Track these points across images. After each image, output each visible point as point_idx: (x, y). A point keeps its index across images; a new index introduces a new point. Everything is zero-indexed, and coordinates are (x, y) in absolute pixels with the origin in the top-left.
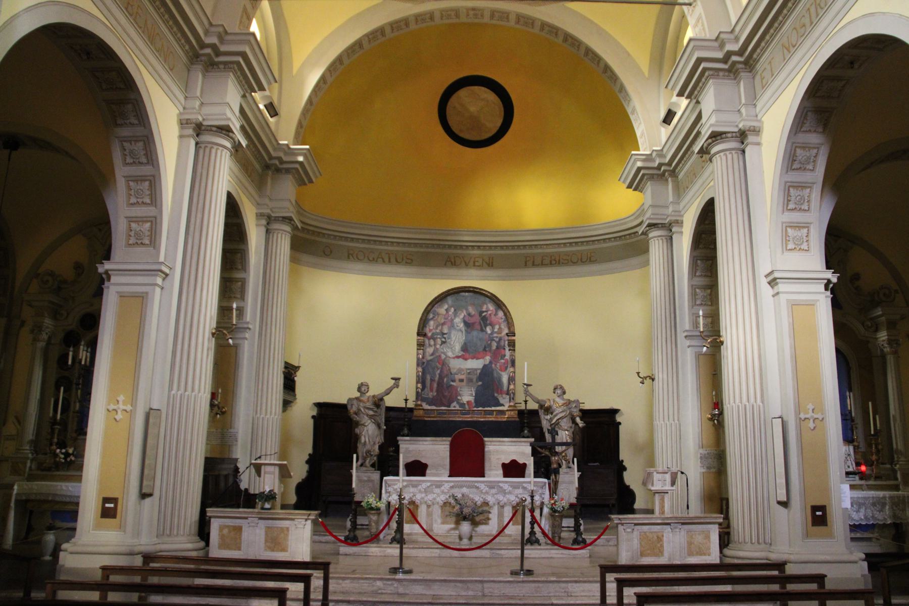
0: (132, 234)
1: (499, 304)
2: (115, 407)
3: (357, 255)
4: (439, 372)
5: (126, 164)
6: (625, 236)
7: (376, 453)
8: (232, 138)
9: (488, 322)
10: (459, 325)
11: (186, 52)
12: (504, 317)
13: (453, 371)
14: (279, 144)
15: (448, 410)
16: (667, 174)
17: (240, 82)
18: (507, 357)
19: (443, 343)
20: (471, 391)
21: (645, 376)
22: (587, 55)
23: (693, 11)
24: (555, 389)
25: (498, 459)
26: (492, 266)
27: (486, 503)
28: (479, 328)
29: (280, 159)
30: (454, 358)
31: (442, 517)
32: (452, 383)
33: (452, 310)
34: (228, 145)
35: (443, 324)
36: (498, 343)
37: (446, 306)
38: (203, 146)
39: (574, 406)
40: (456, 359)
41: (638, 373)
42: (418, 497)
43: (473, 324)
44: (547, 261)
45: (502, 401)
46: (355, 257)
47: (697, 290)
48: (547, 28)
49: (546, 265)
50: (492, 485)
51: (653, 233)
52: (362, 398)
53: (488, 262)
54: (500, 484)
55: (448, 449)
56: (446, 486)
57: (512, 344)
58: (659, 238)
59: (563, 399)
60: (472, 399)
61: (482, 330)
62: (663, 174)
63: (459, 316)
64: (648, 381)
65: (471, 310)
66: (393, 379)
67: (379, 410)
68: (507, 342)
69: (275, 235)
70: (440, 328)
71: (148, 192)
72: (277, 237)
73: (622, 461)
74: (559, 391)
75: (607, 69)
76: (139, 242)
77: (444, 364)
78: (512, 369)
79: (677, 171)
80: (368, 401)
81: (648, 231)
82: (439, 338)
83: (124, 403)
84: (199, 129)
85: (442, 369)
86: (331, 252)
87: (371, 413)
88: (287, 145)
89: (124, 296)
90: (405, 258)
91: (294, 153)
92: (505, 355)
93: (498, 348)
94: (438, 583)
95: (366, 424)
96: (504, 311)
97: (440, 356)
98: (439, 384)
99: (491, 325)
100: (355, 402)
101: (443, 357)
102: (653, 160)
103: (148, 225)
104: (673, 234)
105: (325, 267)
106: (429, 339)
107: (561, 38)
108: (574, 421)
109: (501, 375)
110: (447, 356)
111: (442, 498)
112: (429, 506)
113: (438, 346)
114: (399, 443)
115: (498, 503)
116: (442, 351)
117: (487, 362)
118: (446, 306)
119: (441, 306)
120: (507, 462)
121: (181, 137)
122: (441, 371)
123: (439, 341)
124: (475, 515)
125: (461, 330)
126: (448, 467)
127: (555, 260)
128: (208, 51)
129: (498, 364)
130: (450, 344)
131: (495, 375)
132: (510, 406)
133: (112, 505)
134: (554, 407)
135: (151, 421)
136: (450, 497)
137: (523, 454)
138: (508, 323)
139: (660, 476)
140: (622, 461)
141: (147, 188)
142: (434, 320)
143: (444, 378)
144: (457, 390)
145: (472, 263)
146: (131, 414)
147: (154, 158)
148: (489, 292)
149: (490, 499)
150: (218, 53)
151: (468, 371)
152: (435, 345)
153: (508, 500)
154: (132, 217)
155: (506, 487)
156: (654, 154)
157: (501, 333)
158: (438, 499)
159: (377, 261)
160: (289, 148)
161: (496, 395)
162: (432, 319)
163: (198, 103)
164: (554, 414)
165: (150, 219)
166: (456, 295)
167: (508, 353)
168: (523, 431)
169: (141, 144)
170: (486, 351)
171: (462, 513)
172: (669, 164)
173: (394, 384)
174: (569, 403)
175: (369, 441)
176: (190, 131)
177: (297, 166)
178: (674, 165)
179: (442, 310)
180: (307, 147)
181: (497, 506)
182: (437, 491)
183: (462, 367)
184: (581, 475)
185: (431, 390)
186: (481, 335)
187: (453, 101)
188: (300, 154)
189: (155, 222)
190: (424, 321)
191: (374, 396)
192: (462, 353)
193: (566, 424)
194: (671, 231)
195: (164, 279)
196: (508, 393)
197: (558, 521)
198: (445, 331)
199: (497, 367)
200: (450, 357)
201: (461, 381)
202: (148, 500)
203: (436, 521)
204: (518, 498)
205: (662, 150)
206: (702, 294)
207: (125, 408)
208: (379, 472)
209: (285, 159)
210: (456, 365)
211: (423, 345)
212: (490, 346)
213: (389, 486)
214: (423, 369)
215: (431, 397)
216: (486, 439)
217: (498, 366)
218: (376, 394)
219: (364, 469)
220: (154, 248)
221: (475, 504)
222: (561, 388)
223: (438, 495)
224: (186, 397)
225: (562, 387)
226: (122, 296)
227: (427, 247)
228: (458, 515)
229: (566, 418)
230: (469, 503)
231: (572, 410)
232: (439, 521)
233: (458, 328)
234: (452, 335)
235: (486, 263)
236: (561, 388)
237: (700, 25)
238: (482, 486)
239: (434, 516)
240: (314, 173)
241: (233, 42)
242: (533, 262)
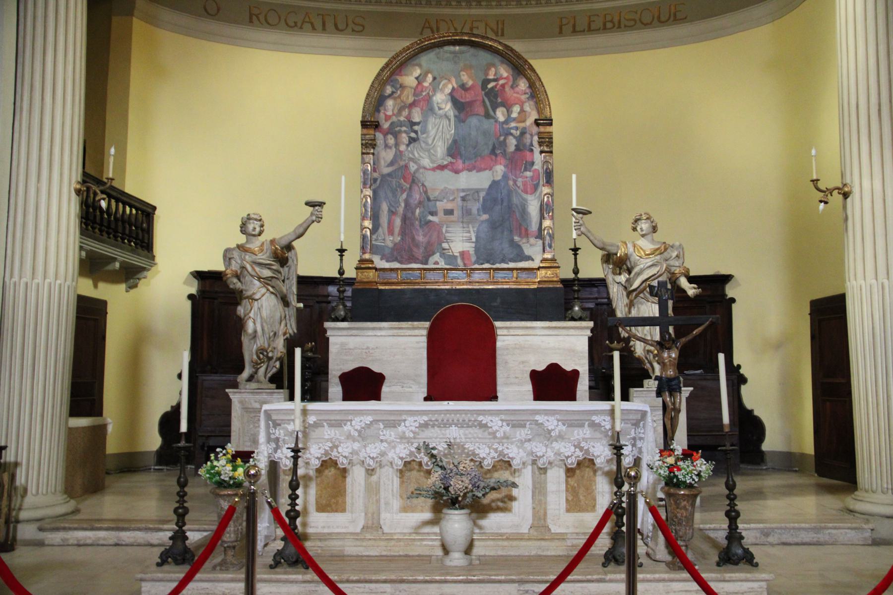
3: (266, 16)
4: (404, 196)
7: (279, 355)
9: (499, 100)
10: (443, 106)
12: (528, 91)
15: (425, 269)
18: (538, 166)
19: (412, 140)
20: (469, 232)
21: (831, 186)
25: (523, 362)
28: (481, 111)
30: (434, 169)
32: (430, 218)
33: (430, 78)
35: (412, 105)
37: (417, 72)
39: (674, 254)
40: (438, 171)
42: (343, 452)
43: (471, 104)
44: (598, 23)
45: (528, 251)
49: (597, 30)
50: (516, 421)
53: (495, 28)
54: (537, 417)
55: (425, 345)
56: (411, 423)
57: (547, 142)
59: (653, 241)
60: (469, 247)
63: (442, 90)
66: (307, 204)
67: (286, 269)
68: (536, 138)
70: (405, 113)
73: (739, 367)
74: (644, 226)
78: (546, 190)
80: (262, 250)
82: (405, 132)
86: (218, 10)
87: (267, 273)
90: (350, 22)
92: (533, 163)
93: (518, 148)
95: (257, 297)
96: (528, 79)
97: (406, 167)
98: (404, 219)
99: (504, 106)
100: (236, 254)
101: (413, 167)
106: (385, 134)
109: (526, 200)
110: (420, 167)
111: (401, 452)
112: (370, 472)
113: (403, 148)
114: (329, 333)
115: (534, 462)
116: (411, 155)
118: (417, 72)
120: (541, 367)
123: (404, 138)
124: (480, 495)
125: (447, 117)
126: (424, 379)
127: (612, 21)
129: (520, 180)
130: (427, 144)
134: (635, 257)
136: (418, 449)
137: (572, 351)
140: (739, 367)
142: (395, 99)
143: (416, 209)
144: (440, 232)
149: (516, 454)
151: (462, 194)
152: (397, 145)
153: (558, 454)
155: (551, 423)
157: (524, 121)
158: (391, 455)
159: (301, 28)
161: (516, 238)
162: (390, 96)
164: (636, 270)
166: (437, 50)
167: (538, 158)
168: (571, 308)
170: (496, 155)
171: (446, 489)
173: (312, 214)
174: (666, 249)
175: (263, 330)
179: (409, 79)
181: (530, 468)
182: (390, 434)
185: (391, 232)
186: (487, 124)
191: (272, 242)
192: (449, 159)
196: (540, 235)
197: (685, 508)
198: (417, 118)
200: (425, 168)
201: (449, 212)
203: (387, 504)
204: (581, 449)
211: (374, 146)
212: (504, 144)
213: (276, 425)
215: (390, 245)
216: (497, 324)
217: (519, 183)
218: (277, 236)
221: (480, 465)
222: (648, 218)
228: (437, 495)
230: (467, 465)
231: (672, 263)
232: (396, 504)
234: (430, 127)
235: (492, 29)
236: (648, 218)
238: (495, 423)
239: (382, 494)
242: (574, 26)
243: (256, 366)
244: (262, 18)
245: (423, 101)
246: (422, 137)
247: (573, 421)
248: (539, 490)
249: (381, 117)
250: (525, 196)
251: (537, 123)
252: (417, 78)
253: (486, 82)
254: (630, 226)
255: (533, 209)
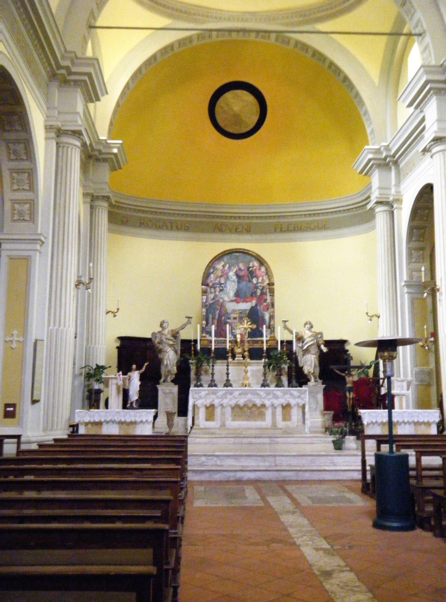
0: (16, 212)
1: (262, 262)
2: (11, 339)
3: (147, 223)
4: (218, 312)
5: (10, 160)
6: (352, 209)
8: (82, 139)
9: (254, 275)
10: (232, 277)
11: (47, 72)
13: (229, 311)
14: (99, 139)
16: (391, 163)
17: (84, 94)
19: (221, 290)
22: (330, 68)
23: (422, 40)
24: (306, 324)
26: (250, 231)
27: (263, 406)
28: (247, 279)
29: (99, 151)
30: (229, 302)
31: (232, 416)
33: (227, 266)
34: (78, 144)
35: (221, 277)
36: (262, 290)
37: (223, 263)
38: (62, 145)
41: (367, 313)
43: (243, 276)
46: (146, 225)
47: (413, 251)
48: (299, 46)
49: (291, 231)
51: (379, 209)
52: (163, 332)
57: (272, 292)
58: (384, 212)
59: (311, 331)
61: (250, 281)
62: (388, 164)
63: (232, 271)
64: (375, 319)
65: (241, 266)
66: (186, 317)
68: (268, 290)
69: (97, 210)
70: (218, 279)
71: (27, 181)
72: (99, 211)
74: (308, 326)
75: (346, 79)
76: (22, 218)
77: (222, 306)
78: (272, 310)
79: (399, 161)
81: (375, 206)
83: (18, 336)
84: (60, 133)
85: (220, 309)
88: (105, 140)
89: (12, 259)
91: (108, 146)
92: (266, 300)
94: (245, 458)
97: (219, 301)
101: (221, 301)
102: (381, 153)
103: (27, 206)
104: (394, 209)
105: (125, 234)
107: (310, 53)
108: (319, 346)
110: (224, 301)
111: (233, 402)
113: (217, 293)
117: (254, 305)
118: (223, 263)
119: (219, 263)
121: (46, 138)
122: (220, 312)
123: (218, 289)
128: (63, 71)
130: (227, 292)
131: (259, 313)
132: (270, 337)
133: (12, 409)
134: (305, 337)
135: (38, 348)
138: (269, 276)
139: (399, 383)
141: (26, 178)
145: (234, 229)
146: (23, 343)
147: (32, 156)
148: (254, 253)
149: (268, 403)
150: (70, 73)
151: (240, 311)
152: (215, 292)
154: (16, 200)
156: (382, 149)
157: (263, 283)
160: (107, 143)
162: (212, 272)
163: (56, 112)
164: (305, 342)
165: (30, 201)
167: (269, 298)
169: (22, 145)
172: (394, 156)
173: (188, 321)
176: (53, 135)
177: (113, 156)
178: (397, 156)
179: (219, 266)
180: (120, 142)
182: (229, 396)
183: (235, 308)
184: (325, 387)
186: (250, 285)
187: (221, 102)
188: (115, 147)
189: (33, 203)
190: (207, 275)
191: (172, 331)
193: (314, 350)
194: (392, 207)
195: (41, 246)
198: (222, 281)
199: (260, 308)
201: (235, 318)
202: (37, 405)
203: (228, 418)
205: (388, 145)
206: (416, 254)
207: (18, 339)
208: (177, 386)
209: (103, 151)
210: (231, 307)
212: (255, 293)
214: (207, 310)
218: (174, 328)
219: (167, 384)
220: (33, 223)
223: (231, 400)
224: (55, 331)
225: (310, 323)
226: (11, 258)
227: (200, 217)
229: (314, 346)
231: (318, 339)
232: (230, 418)
233: (232, 279)
237: (427, 52)
240: (123, 162)
241: (81, 65)
242: (281, 230)
243: (166, 377)
244: (145, 224)
245: (225, 275)
246: (225, 289)
247: (285, 393)
248: (274, 414)
249: (209, 281)
250: (264, 312)
251: (269, 284)
252: (223, 266)
253: (249, 268)
254: (303, 325)
255: (267, 317)
